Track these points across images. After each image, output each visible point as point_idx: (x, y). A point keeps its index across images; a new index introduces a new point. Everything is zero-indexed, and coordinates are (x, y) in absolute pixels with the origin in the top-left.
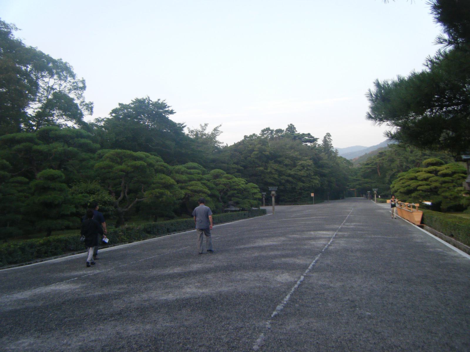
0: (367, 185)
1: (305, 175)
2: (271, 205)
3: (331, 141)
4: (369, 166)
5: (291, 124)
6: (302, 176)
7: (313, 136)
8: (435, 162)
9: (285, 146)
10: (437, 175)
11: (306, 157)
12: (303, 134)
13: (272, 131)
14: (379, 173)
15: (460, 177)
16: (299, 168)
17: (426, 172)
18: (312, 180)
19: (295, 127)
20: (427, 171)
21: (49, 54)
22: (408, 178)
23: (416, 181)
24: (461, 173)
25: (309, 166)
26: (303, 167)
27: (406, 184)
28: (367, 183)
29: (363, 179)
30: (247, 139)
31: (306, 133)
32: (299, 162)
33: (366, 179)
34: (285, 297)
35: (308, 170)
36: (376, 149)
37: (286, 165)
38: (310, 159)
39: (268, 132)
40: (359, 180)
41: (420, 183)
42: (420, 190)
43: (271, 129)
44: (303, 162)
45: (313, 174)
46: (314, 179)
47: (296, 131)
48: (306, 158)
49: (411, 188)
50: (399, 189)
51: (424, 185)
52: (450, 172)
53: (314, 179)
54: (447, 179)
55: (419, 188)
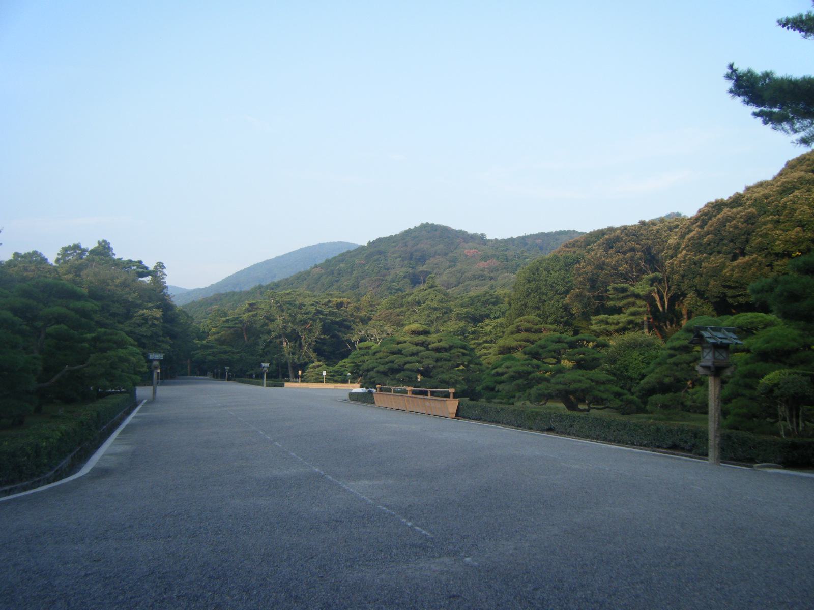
0: (224, 357)
1: (149, 334)
2: (151, 385)
3: (165, 276)
4: (231, 324)
5: (104, 241)
6: (143, 336)
7: (147, 265)
8: (421, 330)
9: (112, 280)
10: (428, 350)
11: (149, 302)
12: (130, 261)
13: (84, 251)
14: (246, 338)
15: (460, 354)
16: (138, 322)
17: (413, 344)
18: (160, 344)
19: (111, 246)
20: (414, 343)
21: (723, 198)
22: (389, 351)
23: (401, 356)
24: (460, 348)
25: (156, 318)
26: (145, 319)
27: (386, 360)
28: (225, 352)
29: (219, 347)
30: (19, 259)
31: (135, 259)
32: (138, 311)
33: (223, 347)
34: (417, 529)
35: (153, 325)
36: (211, 295)
37: (114, 315)
38: (158, 307)
39: (76, 252)
40: (211, 347)
41: (409, 359)
42: (408, 369)
43: (83, 247)
44: (145, 311)
45: (161, 333)
46: (163, 341)
47: (114, 254)
48: (150, 305)
49: (395, 366)
50: (377, 367)
51: (414, 362)
52: (447, 346)
53: (163, 341)
54: (445, 355)
55: (407, 366)
